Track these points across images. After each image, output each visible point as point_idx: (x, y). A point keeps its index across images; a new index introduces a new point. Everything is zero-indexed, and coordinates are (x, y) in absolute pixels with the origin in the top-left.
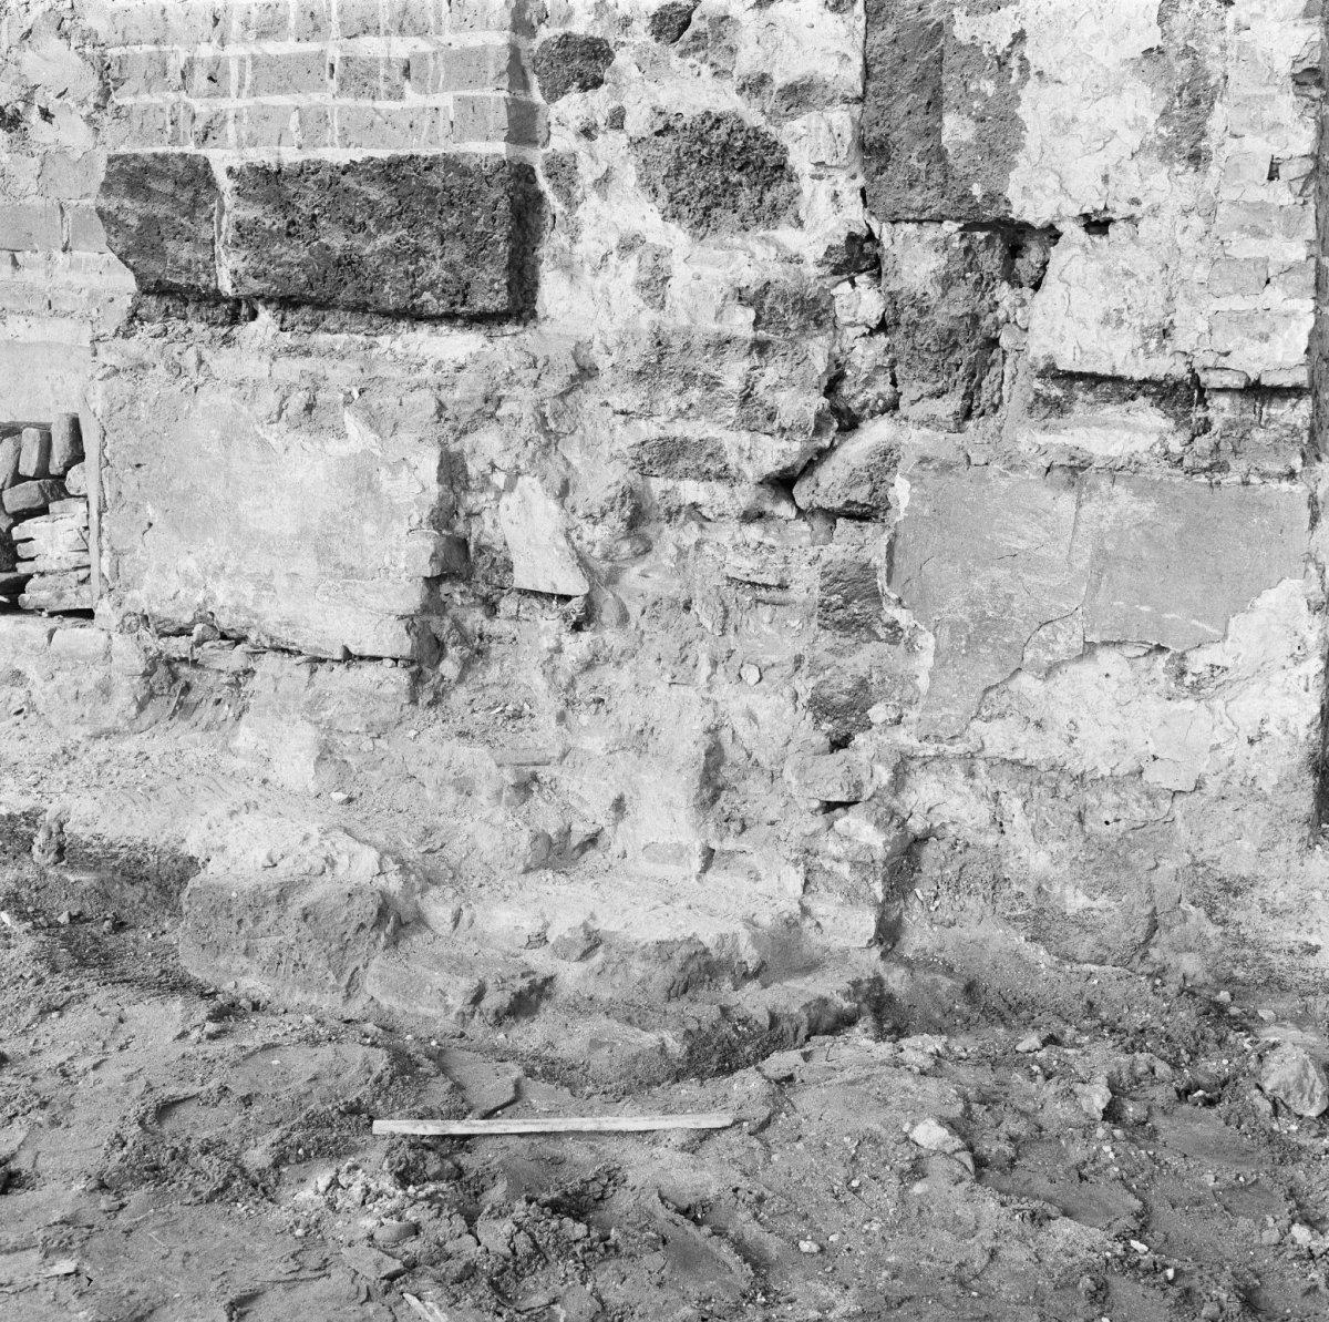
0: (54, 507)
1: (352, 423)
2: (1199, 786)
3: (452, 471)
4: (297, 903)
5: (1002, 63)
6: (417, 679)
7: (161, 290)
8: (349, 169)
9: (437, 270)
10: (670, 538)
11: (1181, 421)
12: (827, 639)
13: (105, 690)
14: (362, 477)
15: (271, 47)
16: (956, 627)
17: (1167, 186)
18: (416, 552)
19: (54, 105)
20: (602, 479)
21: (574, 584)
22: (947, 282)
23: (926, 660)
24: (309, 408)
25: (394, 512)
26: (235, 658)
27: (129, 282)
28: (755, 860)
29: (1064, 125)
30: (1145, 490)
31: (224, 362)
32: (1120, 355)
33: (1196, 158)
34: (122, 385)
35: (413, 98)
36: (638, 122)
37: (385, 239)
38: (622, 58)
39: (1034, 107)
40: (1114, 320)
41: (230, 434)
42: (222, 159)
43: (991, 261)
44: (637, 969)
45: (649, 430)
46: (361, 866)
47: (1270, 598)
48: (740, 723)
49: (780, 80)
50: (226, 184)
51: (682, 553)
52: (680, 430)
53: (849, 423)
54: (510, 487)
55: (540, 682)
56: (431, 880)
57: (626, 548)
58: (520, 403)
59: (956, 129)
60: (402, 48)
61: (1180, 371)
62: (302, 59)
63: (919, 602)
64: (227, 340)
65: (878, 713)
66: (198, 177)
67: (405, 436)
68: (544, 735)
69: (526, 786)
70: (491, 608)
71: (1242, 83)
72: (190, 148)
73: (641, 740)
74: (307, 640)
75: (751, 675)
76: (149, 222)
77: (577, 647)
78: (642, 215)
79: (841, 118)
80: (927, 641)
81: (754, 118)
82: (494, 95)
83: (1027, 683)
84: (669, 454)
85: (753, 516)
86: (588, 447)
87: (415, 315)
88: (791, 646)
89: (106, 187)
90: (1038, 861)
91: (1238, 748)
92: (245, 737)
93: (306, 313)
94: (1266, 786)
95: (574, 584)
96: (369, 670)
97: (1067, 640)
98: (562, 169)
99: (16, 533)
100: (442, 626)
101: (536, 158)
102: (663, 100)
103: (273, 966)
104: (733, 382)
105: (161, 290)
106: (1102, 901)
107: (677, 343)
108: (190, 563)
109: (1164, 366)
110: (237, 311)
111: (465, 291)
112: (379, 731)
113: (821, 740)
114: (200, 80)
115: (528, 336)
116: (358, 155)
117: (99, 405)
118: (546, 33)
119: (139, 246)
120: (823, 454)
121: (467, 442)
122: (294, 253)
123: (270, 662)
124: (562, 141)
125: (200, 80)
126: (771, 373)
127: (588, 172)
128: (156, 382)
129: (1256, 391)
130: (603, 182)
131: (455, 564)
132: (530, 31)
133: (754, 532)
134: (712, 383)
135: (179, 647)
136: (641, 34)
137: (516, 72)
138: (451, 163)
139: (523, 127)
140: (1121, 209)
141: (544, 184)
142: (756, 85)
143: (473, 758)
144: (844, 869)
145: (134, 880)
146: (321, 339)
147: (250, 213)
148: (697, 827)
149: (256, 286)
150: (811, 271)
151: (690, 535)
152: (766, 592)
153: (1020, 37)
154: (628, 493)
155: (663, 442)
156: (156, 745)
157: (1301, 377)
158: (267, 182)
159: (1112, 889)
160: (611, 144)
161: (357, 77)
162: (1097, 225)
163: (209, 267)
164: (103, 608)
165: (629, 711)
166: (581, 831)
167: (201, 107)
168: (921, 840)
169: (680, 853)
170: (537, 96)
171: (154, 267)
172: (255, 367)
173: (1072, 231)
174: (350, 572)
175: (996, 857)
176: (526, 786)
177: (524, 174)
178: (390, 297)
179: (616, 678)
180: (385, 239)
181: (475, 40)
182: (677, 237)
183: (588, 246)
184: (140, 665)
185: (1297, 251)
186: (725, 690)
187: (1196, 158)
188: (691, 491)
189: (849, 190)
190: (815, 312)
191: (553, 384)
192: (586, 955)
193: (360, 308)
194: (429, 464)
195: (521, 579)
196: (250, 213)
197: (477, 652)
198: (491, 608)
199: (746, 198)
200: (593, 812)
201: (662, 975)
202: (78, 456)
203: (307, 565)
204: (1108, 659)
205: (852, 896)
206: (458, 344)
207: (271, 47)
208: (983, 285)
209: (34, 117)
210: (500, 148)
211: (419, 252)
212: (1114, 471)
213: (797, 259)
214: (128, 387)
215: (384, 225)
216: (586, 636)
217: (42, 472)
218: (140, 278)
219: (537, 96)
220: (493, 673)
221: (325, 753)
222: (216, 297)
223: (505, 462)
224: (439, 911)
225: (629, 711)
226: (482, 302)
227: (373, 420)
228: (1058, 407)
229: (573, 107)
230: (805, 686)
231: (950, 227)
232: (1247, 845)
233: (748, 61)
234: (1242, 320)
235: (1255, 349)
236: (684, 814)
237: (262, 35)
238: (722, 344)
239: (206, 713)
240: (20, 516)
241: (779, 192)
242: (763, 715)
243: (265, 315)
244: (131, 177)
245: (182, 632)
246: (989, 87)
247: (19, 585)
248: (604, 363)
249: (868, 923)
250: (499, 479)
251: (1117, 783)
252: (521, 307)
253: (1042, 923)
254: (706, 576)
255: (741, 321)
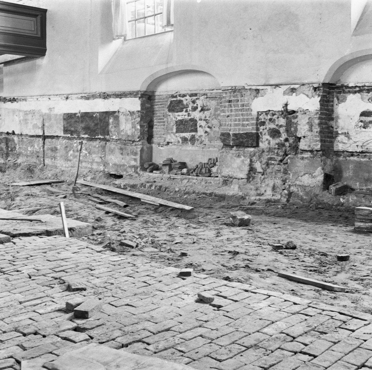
0: (215, 166)
1: (242, 157)
2: (314, 186)
3: (251, 161)
4: (235, 196)
5: (296, 123)
6: (248, 180)
7: (225, 145)
8: (242, 133)
9: (250, 142)
10: (271, 167)
11: (312, 154)
12: (284, 175)
13: (219, 183)
14: (243, 161)
15: (236, 123)
16: (294, 173)
17: (309, 133)
18: (247, 168)
19: (215, 126)
20: (264, 161)
21: (262, 171)
22: (293, 142)
23: (291, 176)
24: (238, 155)
25: (246, 165)
26: (231, 180)
27: (222, 144)
28: (277, 195)
29: (301, 129)
30: (309, 160)
31: (231, 152)
32: (306, 148)
33: (312, 131)
34: (222, 154)
35: (248, 127)
36: (268, 129)
37: (245, 140)
38: (267, 123)
39: (299, 127)
40: (306, 145)
41: (232, 158)
42: (231, 133)
43: (297, 140)
44: (263, 201)
45: (269, 156)
46: (241, 194)
47: (318, 169)
48: (276, 183)
49: (279, 125)
50: (231, 135)
51: (272, 168)
52: (272, 156)
53: (287, 155)
54: (256, 162)
55: (259, 180)
56: (247, 196)
57: (267, 167)
58: (257, 154)
59: (292, 129)
60: (247, 123)
61: (311, 149)
62: (238, 124)
63: (291, 171)
64: (231, 149)
65: (287, 181)
66: (229, 134)
67: (247, 158)
68: (259, 185)
69: (257, 189)
70: (255, 174)
71: (314, 125)
72: (228, 132)
73: (268, 185)
74: (238, 177)
75: (277, 179)
76: (224, 139)
77: (263, 177)
78: (268, 137)
79: (284, 128)
80: (291, 174)
81: (277, 128)
82: (255, 127)
83: (300, 178)
84: (271, 159)
85: (278, 164)
86: (264, 158)
87: (248, 147)
88: (281, 176)
89: (221, 136)
90: (301, 194)
91: (317, 183)
92: (232, 187)
93: (239, 147)
94: (319, 186)
95: (262, 171)
96: (243, 180)
97: (302, 173)
98: (261, 133)
99: (211, 169)
100: (250, 175)
101: (259, 132)
102: (270, 127)
103: (233, 202)
104: (276, 152)
105: (225, 145)
106: (307, 197)
107: (271, 148)
108: (227, 171)
109: (310, 149)
110: (232, 147)
111: (252, 144)
112: (244, 185)
113: (283, 184)
114: (229, 125)
115: (258, 148)
116: (243, 132)
117: (219, 156)
118: (260, 121)
119: (223, 141)
120: (285, 158)
121: (252, 158)
122: (238, 141)
123: (235, 180)
124: (261, 131)
125: (229, 125)
126: (279, 151)
127: (263, 133)
128: (224, 154)
129: (317, 151)
130: (265, 134)
131: (251, 170)
132: (258, 121)
133: (279, 166)
134: (274, 152)
135: (226, 179)
136: (268, 121)
137: (257, 124)
138: (251, 133)
139: (258, 129)
140: (306, 136)
141: (260, 134)
142: (277, 125)
143: (252, 187)
144: (284, 195)
145: (221, 198)
146: (240, 149)
147: (234, 138)
148: (272, 192)
149: (234, 144)
150: (283, 141)
151: (273, 166)
152: (279, 171)
153: (297, 121)
154: (267, 162)
155: (270, 158)
156: (224, 188)
157: (320, 149)
158: (235, 135)
159: (308, 196)
160: (265, 131)
161: (243, 125)
162: (304, 137)
163: (230, 143)
164: (219, 176)
165: (267, 183)
166: (262, 193)
167: (229, 128)
168: (292, 193)
169: (270, 195)
170: (259, 127)
171: (225, 143)
172: (234, 152)
173: (302, 137)
174: (242, 171)
175: (298, 194)
176: (257, 189)
177: (257, 134)
178: (246, 145)
179: (266, 180)
180: (245, 140)
181: (253, 122)
182: (271, 139)
183: (264, 140)
184: (222, 181)
185: (319, 139)
186: (275, 180)
187: (312, 131)
188: (273, 162)
189: (286, 134)
190: (283, 145)
191: (260, 153)
192: (259, 201)
193: (243, 146)
194: (249, 160)
195: (258, 171)
196: (234, 138)
197: (254, 178)
198: (255, 174)
199: (277, 135)
200: (263, 192)
201: (265, 202)
202: (217, 161)
203: (238, 170)
204: (307, 175)
205: (285, 197)
206: (252, 149)
207: (236, 123)
208: (297, 142)
209: (213, 128)
210: (255, 131)
211: (249, 141)
212: (306, 158)
213: (281, 140)
214: (218, 348)
215: (245, 139)
216: (263, 176)
217: (213, 163)
218: (224, 144)
219: (259, 127)
220: (255, 180)
221: (239, 187)
222: (230, 145)
223: (256, 160)
224: (247, 198)
225: (267, 183)
226: (254, 145)
227: (244, 156)
228: (302, 153)
229: (262, 127)
230: (281, 179)
231: (294, 137)
232: (318, 191)
233: (277, 123)
234: (315, 145)
235: (316, 147)
236: (271, 191)
237: (235, 121)
238: (275, 148)
239: (229, 185)
240: (211, 167)
241: (280, 134)
242: (279, 182)
243: (235, 147)
244: (223, 134)
245: (227, 177)
246: (295, 126)
247: (211, 174)
248: (265, 150)
249: (286, 199)
250: (255, 161)
251: (308, 186)
252: (257, 146)
253: (302, 199)
254: (274, 170)
255: (277, 146)
